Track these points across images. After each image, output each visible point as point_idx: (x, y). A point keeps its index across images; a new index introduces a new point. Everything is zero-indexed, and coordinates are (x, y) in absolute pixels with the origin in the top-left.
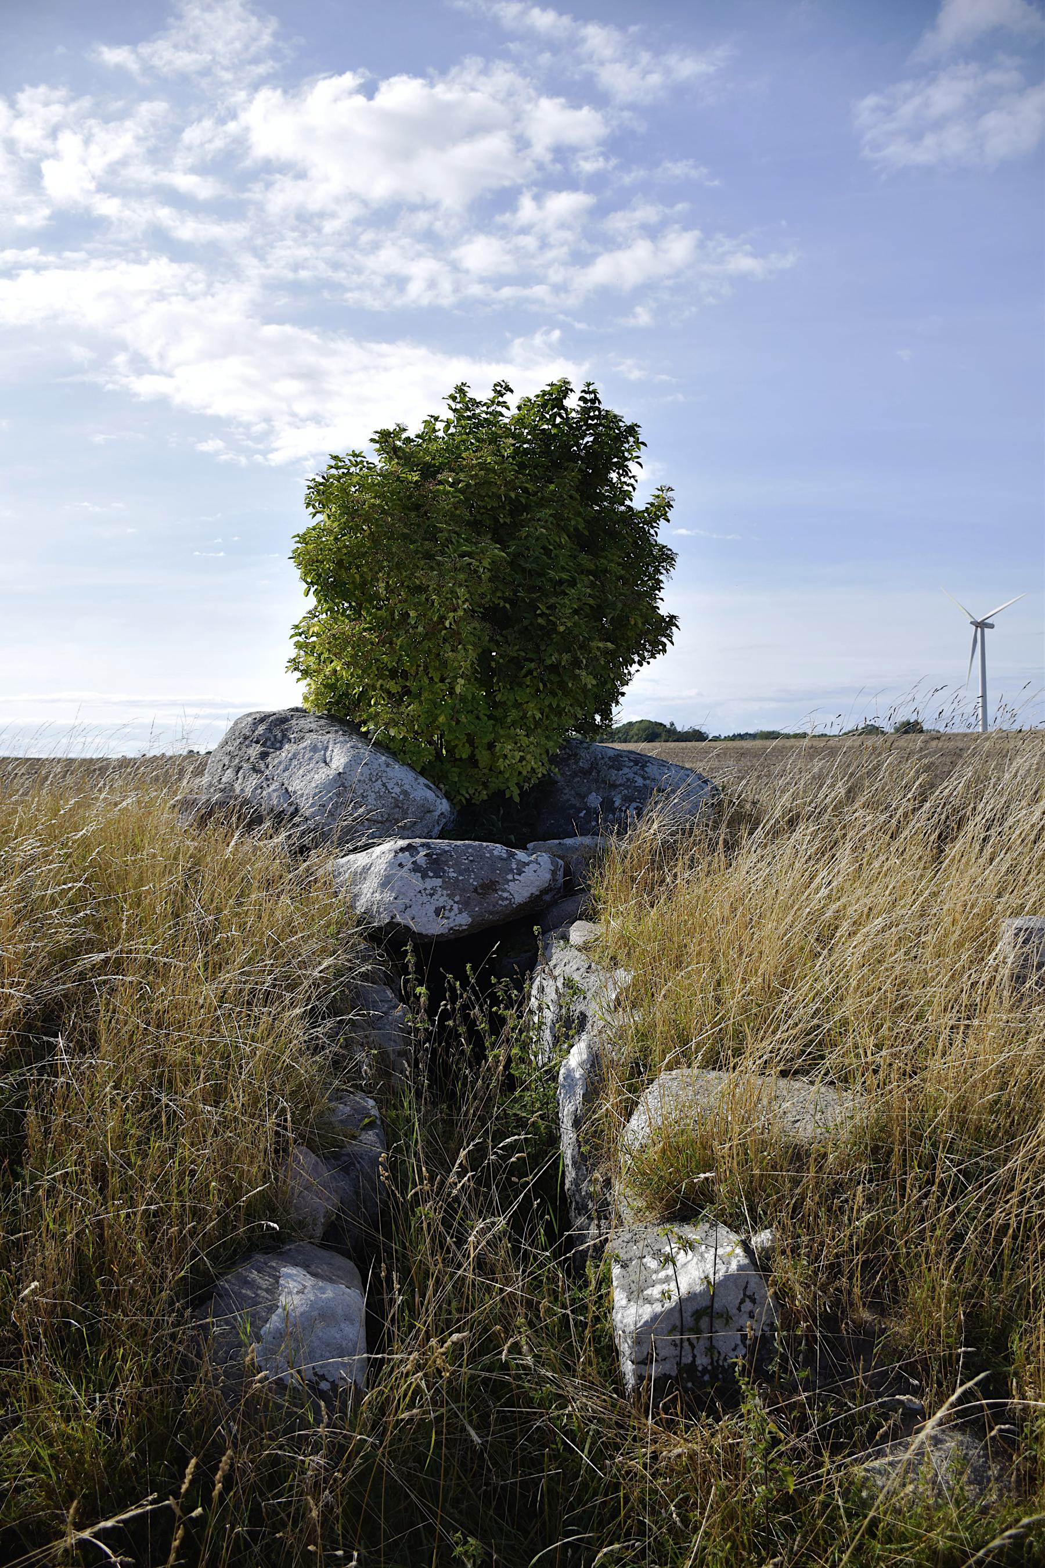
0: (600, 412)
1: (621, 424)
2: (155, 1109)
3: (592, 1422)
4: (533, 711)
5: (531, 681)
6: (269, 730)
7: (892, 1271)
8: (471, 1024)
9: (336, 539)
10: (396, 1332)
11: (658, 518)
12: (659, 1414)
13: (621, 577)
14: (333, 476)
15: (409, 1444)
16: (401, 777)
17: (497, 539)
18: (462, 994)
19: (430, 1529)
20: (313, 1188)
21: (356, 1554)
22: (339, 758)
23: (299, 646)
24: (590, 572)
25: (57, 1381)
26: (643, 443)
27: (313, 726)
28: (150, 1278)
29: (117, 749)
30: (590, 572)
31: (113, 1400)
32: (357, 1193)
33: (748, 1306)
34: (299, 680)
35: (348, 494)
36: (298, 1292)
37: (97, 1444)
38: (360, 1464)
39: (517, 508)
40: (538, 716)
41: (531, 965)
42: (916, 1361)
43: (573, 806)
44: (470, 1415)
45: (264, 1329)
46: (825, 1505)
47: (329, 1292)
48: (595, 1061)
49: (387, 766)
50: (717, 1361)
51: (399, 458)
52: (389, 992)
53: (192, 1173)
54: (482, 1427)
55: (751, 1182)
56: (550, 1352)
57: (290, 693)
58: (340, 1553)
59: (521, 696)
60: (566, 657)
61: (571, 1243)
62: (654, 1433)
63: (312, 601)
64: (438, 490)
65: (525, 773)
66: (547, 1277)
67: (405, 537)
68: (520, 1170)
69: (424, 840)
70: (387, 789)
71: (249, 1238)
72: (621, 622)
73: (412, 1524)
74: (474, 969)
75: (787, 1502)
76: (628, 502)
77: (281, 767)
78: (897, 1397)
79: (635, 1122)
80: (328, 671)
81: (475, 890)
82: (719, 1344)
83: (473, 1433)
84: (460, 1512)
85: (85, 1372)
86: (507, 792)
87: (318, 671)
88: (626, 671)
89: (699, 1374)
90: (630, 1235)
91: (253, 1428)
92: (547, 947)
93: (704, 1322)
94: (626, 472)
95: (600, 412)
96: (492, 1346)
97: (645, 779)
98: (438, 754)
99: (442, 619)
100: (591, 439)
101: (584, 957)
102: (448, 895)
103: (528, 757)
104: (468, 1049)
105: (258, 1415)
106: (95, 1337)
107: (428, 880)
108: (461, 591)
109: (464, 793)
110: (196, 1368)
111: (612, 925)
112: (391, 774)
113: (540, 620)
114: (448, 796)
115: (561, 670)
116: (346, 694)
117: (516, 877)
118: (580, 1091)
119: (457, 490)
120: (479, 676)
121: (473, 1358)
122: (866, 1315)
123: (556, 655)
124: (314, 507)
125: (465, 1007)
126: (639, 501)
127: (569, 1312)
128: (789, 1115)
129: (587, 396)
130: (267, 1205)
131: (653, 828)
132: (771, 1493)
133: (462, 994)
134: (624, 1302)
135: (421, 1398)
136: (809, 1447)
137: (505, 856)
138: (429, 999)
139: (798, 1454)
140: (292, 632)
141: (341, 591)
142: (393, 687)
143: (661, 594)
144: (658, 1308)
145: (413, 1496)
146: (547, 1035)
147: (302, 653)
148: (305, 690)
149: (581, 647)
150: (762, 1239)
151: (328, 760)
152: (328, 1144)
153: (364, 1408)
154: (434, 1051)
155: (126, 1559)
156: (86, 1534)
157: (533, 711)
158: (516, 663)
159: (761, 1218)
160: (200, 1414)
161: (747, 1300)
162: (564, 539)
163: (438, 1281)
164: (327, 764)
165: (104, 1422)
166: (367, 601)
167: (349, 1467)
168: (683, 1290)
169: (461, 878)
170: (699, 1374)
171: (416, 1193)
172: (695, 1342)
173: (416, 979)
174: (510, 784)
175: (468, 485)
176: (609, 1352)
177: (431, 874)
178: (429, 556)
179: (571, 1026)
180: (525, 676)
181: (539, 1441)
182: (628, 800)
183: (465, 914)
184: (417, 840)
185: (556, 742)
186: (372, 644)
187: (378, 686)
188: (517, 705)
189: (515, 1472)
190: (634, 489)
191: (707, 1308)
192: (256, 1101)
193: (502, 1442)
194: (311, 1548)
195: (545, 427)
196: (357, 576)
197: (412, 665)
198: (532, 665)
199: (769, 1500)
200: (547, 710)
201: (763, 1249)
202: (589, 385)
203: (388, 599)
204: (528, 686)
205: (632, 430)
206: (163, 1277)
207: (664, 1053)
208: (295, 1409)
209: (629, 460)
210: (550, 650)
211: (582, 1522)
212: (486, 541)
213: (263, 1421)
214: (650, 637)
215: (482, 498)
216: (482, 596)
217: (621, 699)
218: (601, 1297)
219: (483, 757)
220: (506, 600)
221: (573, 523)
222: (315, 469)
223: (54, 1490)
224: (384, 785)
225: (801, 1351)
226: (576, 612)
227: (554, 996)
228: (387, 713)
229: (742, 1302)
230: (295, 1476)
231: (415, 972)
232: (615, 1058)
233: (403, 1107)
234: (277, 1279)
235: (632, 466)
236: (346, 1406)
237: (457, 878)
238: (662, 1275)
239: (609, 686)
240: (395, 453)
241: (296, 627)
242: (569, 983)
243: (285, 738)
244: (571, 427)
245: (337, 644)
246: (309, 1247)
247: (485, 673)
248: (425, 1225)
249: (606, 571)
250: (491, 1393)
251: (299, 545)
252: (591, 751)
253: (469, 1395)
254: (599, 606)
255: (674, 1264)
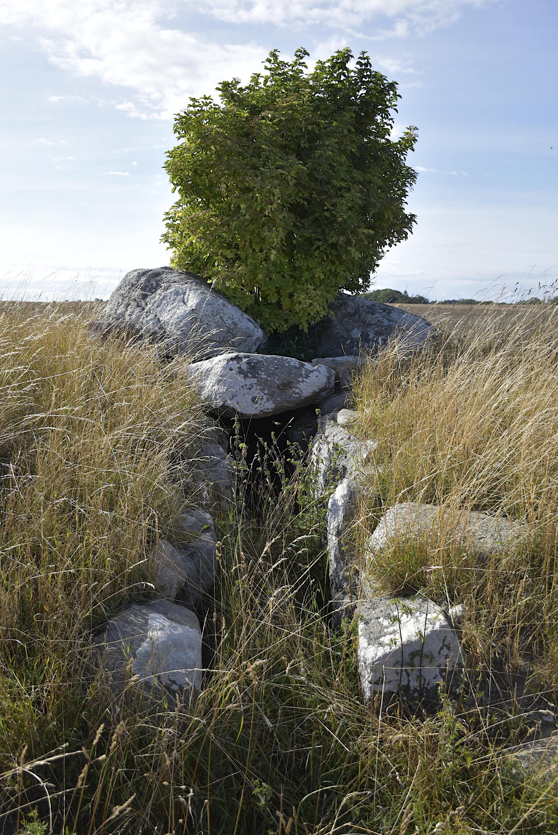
0: (371, 73)
1: (385, 82)
2: (71, 513)
3: (342, 718)
4: (319, 274)
5: (319, 254)
6: (148, 280)
7: (540, 635)
8: (273, 470)
9: (193, 155)
10: (221, 656)
11: (407, 148)
12: (385, 715)
13: (379, 188)
14: (191, 112)
15: (227, 726)
16: (232, 313)
17: (299, 156)
18: (268, 450)
19: (239, 778)
20: (171, 567)
21: (192, 790)
22: (193, 300)
23: (168, 225)
24: (360, 183)
25: (8, 677)
26: (399, 95)
27: (177, 279)
28: (67, 617)
29: (48, 297)
30: (360, 183)
31: (42, 689)
32: (198, 571)
33: (445, 651)
34: (168, 248)
35: (202, 125)
36: (160, 629)
37: (32, 714)
38: (196, 736)
39: (313, 137)
40: (322, 277)
41: (314, 433)
42: (552, 692)
43: (342, 337)
44: (265, 709)
45: (138, 651)
46: (490, 777)
47: (180, 630)
48: (351, 495)
49: (224, 306)
50: (423, 685)
51: (235, 101)
52: (221, 449)
53: (94, 553)
54: (273, 716)
55: (451, 574)
56: (317, 673)
57: (162, 257)
58: (183, 787)
59: (312, 263)
60: (342, 238)
61: (331, 608)
62: (382, 726)
63: (177, 196)
64: (262, 123)
65: (312, 314)
66: (317, 628)
67: (239, 154)
68: (303, 559)
69: (246, 354)
70: (223, 320)
71: (130, 595)
72: (379, 217)
73: (227, 774)
74: (276, 435)
75: (466, 773)
76: (387, 137)
77: (155, 305)
78: (540, 711)
79: (377, 533)
80: (187, 242)
81: (278, 387)
82: (425, 674)
83: (267, 721)
84: (257, 768)
85: (26, 672)
86: (300, 326)
87: (180, 243)
88: (380, 250)
89: (411, 692)
90: (371, 604)
91: (130, 711)
92: (323, 424)
93: (417, 660)
94: (387, 115)
95: (371, 73)
96: (280, 668)
97: (389, 321)
98: (257, 301)
99: (263, 209)
100: (365, 92)
101: (346, 432)
102: (260, 389)
103: (315, 303)
104: (270, 485)
105: (133, 703)
106: (32, 651)
107: (248, 379)
108: (277, 191)
109: (272, 325)
110: (94, 673)
111: (367, 410)
112: (226, 311)
113: (326, 214)
114: (262, 327)
115: (338, 247)
116: (198, 259)
117: (305, 380)
118: (341, 514)
119: (274, 124)
120: (285, 249)
121: (269, 675)
122: (521, 662)
123: (336, 237)
124: (179, 133)
125: (270, 459)
126: (395, 136)
127: (330, 649)
128: (477, 534)
129: (363, 61)
130: (142, 574)
131: (395, 350)
132: (456, 767)
133: (268, 450)
134: (366, 645)
135: (235, 697)
136: (480, 740)
137: (298, 366)
138: (248, 451)
139: (474, 745)
140: (165, 217)
141: (196, 190)
142: (230, 254)
143: (406, 200)
144: (387, 650)
145: (228, 757)
146: (321, 479)
147: (171, 231)
148: (172, 255)
149: (353, 232)
150: (456, 610)
151: (186, 301)
152: (181, 541)
153: (200, 701)
154: (249, 486)
155: (50, 784)
156: (27, 768)
157: (319, 274)
158: (309, 241)
159: (456, 597)
160: (97, 701)
161: (445, 648)
162: (344, 159)
163: (248, 628)
164: (185, 303)
165: (37, 702)
166: (213, 197)
167: (189, 737)
168: (405, 639)
169: (269, 379)
170: (411, 692)
171: (236, 569)
172: (410, 672)
173: (240, 439)
174: (302, 321)
175: (280, 121)
176: (354, 676)
177: (250, 376)
178: (255, 168)
179: (336, 475)
180: (315, 250)
181: (308, 728)
182: (378, 334)
183: (271, 402)
184: (242, 354)
185: (333, 294)
186: (216, 225)
187: (220, 253)
188: (309, 269)
189: (292, 746)
190: (392, 128)
191: (418, 651)
192: (136, 509)
193: (285, 727)
194: (165, 783)
195: (334, 82)
196: (207, 181)
197: (242, 241)
198: (320, 243)
199: (454, 772)
200: (328, 273)
201: (456, 616)
202: (363, 53)
203: (227, 197)
204: (316, 257)
205: (392, 86)
206: (75, 616)
207: (397, 492)
208: (156, 701)
209: (389, 107)
210: (332, 233)
211: (334, 778)
212: (293, 159)
213: (136, 707)
214: (397, 228)
215: (289, 130)
216: (289, 196)
217: (376, 269)
218: (350, 642)
219: (286, 302)
220: (304, 199)
221: (349, 148)
222: (181, 106)
223: (5, 742)
224: (221, 318)
225: (478, 681)
226: (350, 209)
227: (326, 455)
228: (225, 271)
229: (442, 648)
230: (155, 741)
231: (239, 434)
232: (365, 494)
233: (229, 519)
234: (146, 621)
235: (390, 110)
236: (188, 701)
237: (266, 379)
238: (391, 629)
239: (369, 259)
240: (232, 98)
241: (167, 213)
242: (336, 447)
243: (158, 286)
244: (351, 84)
245: (194, 225)
246: (167, 602)
247: (289, 248)
248: (241, 591)
249: (370, 182)
250: (280, 696)
251: (169, 159)
252: (355, 301)
253: (265, 697)
254: (365, 206)
255: (400, 622)
